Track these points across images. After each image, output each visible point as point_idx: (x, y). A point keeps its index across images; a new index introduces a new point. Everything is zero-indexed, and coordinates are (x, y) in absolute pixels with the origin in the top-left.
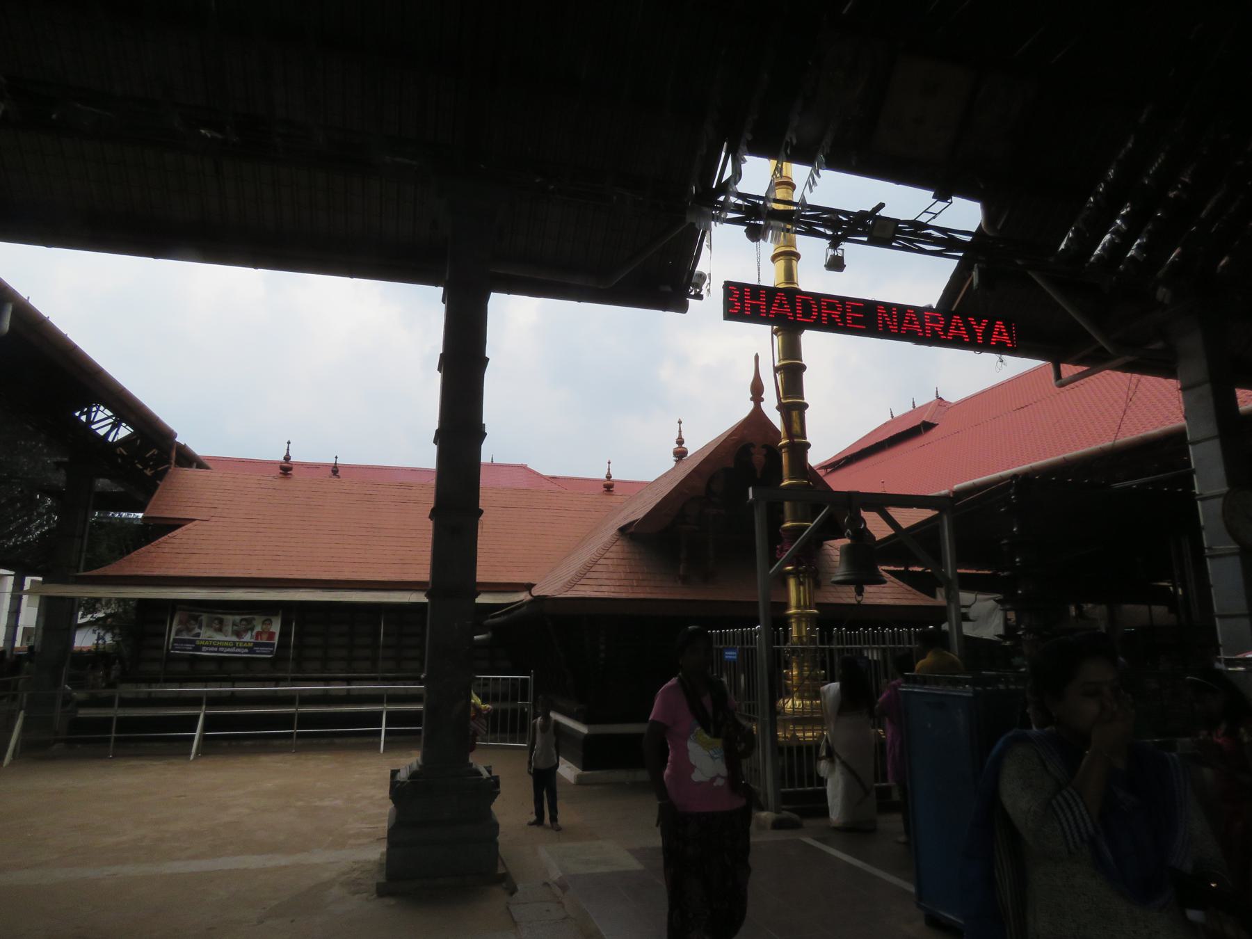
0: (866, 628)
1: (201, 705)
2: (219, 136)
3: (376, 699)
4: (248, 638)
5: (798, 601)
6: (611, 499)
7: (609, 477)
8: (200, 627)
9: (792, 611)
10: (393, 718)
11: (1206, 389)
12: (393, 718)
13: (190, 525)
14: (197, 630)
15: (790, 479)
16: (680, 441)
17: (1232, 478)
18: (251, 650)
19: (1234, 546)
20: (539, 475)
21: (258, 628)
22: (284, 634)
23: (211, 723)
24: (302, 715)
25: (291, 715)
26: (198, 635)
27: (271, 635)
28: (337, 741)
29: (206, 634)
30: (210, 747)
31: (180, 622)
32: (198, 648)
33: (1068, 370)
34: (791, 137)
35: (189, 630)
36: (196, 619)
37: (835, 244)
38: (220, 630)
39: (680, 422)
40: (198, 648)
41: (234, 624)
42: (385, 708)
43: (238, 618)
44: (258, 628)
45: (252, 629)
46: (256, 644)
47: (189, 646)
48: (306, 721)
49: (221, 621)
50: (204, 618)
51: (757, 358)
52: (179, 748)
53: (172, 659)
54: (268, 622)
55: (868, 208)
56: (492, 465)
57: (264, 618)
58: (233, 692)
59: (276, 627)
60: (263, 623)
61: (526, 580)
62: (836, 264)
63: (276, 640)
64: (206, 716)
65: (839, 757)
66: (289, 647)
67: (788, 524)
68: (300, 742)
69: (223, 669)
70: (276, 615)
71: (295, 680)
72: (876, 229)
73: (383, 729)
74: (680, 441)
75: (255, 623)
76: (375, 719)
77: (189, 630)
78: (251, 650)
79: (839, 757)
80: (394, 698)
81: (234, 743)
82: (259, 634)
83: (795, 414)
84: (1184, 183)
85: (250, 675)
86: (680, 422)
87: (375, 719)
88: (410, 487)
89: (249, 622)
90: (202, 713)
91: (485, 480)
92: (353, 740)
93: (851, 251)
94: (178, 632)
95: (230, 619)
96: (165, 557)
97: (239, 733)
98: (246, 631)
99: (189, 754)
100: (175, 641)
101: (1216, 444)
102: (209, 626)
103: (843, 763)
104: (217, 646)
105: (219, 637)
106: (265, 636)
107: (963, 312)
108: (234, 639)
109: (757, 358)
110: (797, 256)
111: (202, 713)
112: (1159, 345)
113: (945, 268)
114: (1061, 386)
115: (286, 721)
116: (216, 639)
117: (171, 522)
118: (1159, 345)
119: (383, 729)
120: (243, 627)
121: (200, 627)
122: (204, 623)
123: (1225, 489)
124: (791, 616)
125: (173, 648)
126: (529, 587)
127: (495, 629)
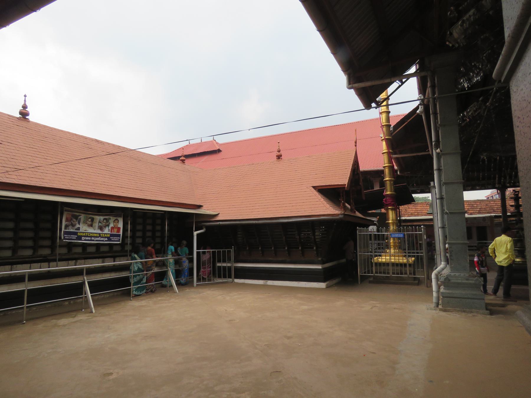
4: (106, 231)
18: (109, 239)
21: (112, 225)
26: (78, 229)
27: (119, 228)
29: (84, 228)
31: (67, 220)
35: (73, 225)
38: (91, 226)
40: (79, 238)
41: (100, 222)
43: (102, 218)
44: (112, 225)
45: (108, 226)
46: (112, 235)
49: (93, 220)
50: (82, 217)
53: (70, 246)
59: (121, 225)
60: (114, 222)
69: (99, 251)
75: (110, 221)
77: (73, 225)
82: (112, 228)
95: (98, 218)
97: (117, 289)
98: (105, 227)
102: (85, 222)
105: (90, 230)
106: (116, 230)
116: (90, 231)
125: (64, 239)
126: (199, 207)
127: (207, 228)
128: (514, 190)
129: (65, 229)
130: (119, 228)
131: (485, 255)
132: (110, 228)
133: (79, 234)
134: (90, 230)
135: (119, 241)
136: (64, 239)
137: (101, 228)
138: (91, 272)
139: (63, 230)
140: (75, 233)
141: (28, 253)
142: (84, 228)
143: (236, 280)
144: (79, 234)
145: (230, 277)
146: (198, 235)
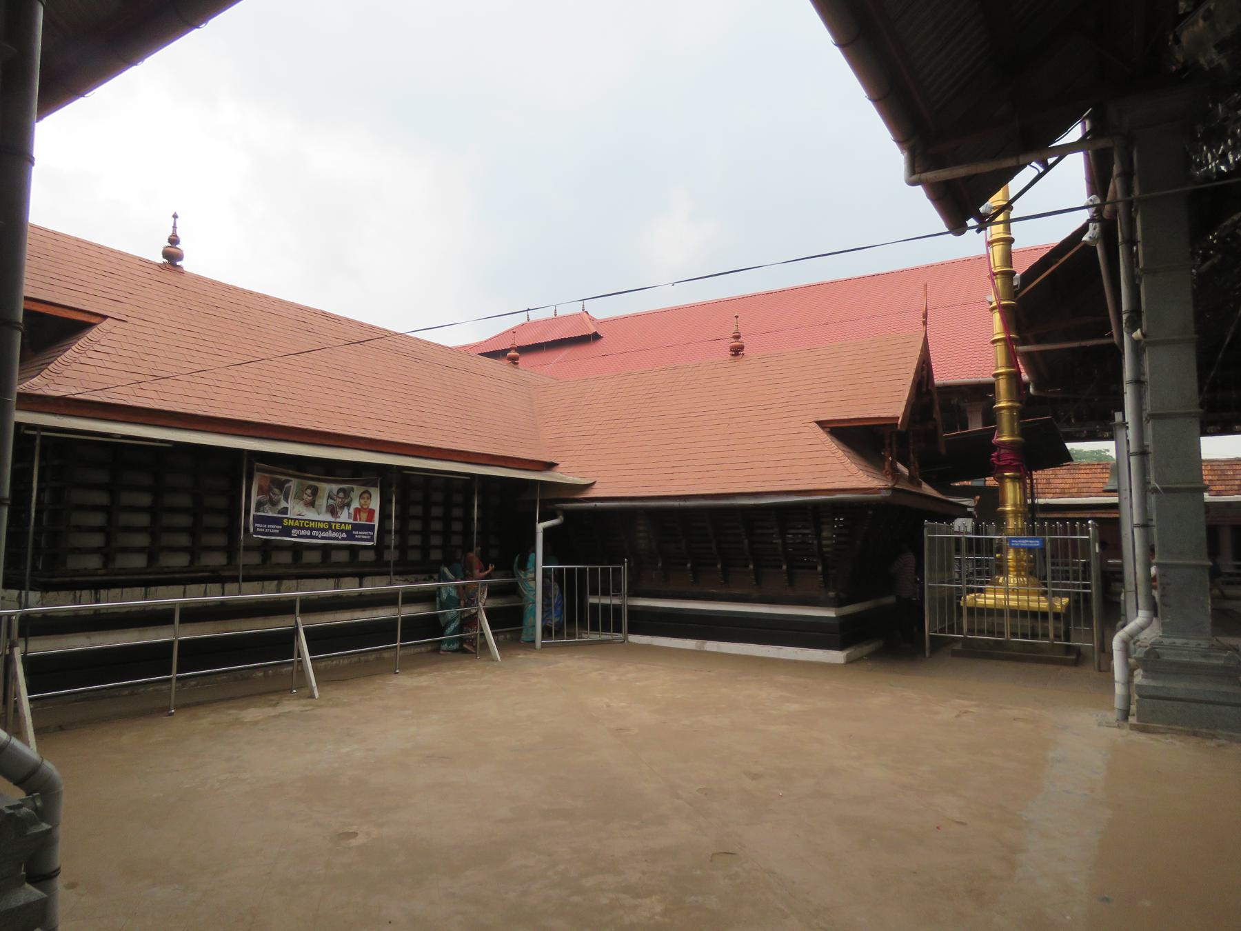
3: (285, 608)
4: (345, 517)
13: (106, 325)
14: (283, 504)
16: (174, 240)
18: (350, 536)
21: (356, 504)
22: (384, 516)
26: (285, 511)
27: (372, 512)
29: (296, 510)
31: (261, 491)
32: (287, 531)
35: (274, 503)
36: (281, 485)
38: (312, 504)
39: (175, 216)
40: (287, 531)
41: (330, 497)
42: (302, 623)
43: (335, 487)
44: (356, 504)
45: (348, 505)
46: (356, 527)
47: (276, 528)
48: (195, 654)
49: (315, 491)
50: (293, 484)
52: (294, 684)
54: (366, 495)
56: (32, 226)
57: (363, 489)
58: (96, 610)
61: (547, 458)
66: (390, 532)
69: (326, 562)
74: (174, 240)
75: (353, 495)
76: (282, 645)
77: (274, 503)
80: (311, 606)
82: (357, 511)
86: (175, 216)
91: (31, 246)
94: (260, 505)
95: (327, 488)
98: (342, 507)
102: (298, 497)
105: (310, 515)
106: (364, 515)
108: (329, 518)
116: (310, 515)
125: (256, 532)
126: (550, 466)
127: (568, 514)
129: (257, 510)
130: (372, 512)
132: (352, 510)
133: (286, 523)
134: (310, 515)
137: (333, 511)
139: (253, 512)
142: (296, 510)
144: (286, 523)
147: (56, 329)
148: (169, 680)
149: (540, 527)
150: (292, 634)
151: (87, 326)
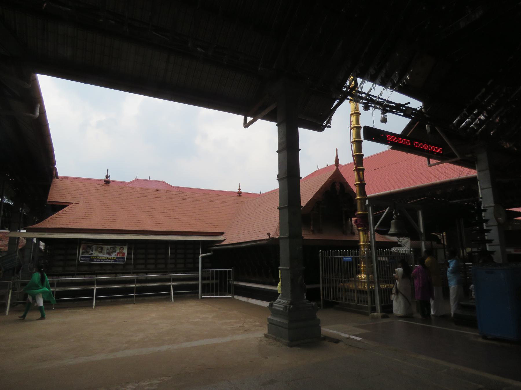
0: (343, 250)
1: (94, 285)
2: (203, 51)
3: (168, 280)
4: (113, 255)
5: (364, 240)
6: (240, 199)
7: (240, 190)
8: (92, 251)
9: (361, 244)
10: (176, 288)
11: (488, 172)
12: (176, 288)
13: (71, 206)
15: (360, 196)
17: (495, 202)
18: (115, 261)
19: (496, 223)
20: (170, 186)
21: (118, 251)
22: (129, 254)
23: (99, 292)
24: (137, 288)
25: (133, 288)
26: (92, 254)
27: (124, 254)
28: (146, 298)
29: (95, 254)
30: (101, 302)
31: (83, 249)
32: (92, 260)
33: (433, 161)
34: (372, 71)
35: (87, 252)
37: (383, 113)
38: (101, 252)
40: (92, 260)
41: (107, 250)
42: (172, 284)
43: (109, 247)
44: (118, 251)
45: (115, 252)
46: (117, 258)
48: (139, 290)
49: (102, 248)
50: (94, 247)
51: (337, 150)
52: (168, 297)
53: (80, 265)
55: (403, 103)
59: (125, 251)
60: (120, 249)
62: (384, 121)
63: (126, 256)
64: (97, 289)
65: (401, 293)
66: (131, 259)
67: (359, 213)
68: (137, 299)
69: (103, 268)
70: (125, 245)
71: (123, 273)
72: (387, 107)
73: (94, 297)
75: (116, 249)
77: (87, 252)
78: (115, 261)
79: (401, 293)
80: (175, 280)
81: (102, 301)
82: (118, 253)
83: (361, 173)
84: (493, 105)
85: (104, 272)
87: (168, 288)
88: (161, 191)
89: (114, 248)
90: (95, 288)
91: (56, 183)
92: (153, 298)
93: (389, 116)
95: (105, 247)
96: (59, 220)
97: (115, 295)
98: (113, 252)
99: (92, 306)
100: (82, 257)
101: (491, 189)
102: (96, 250)
103: (403, 295)
104: (100, 259)
105: (101, 255)
106: (121, 255)
107: (412, 139)
108: (108, 256)
109: (337, 150)
110: (360, 114)
111: (95, 288)
112: (470, 156)
113: (406, 121)
114: (431, 166)
115: (131, 290)
116: (100, 256)
117: (61, 204)
118: (470, 156)
119: (94, 297)
120: (111, 251)
121: (92, 251)
122: (94, 249)
123: (493, 205)
124: (361, 245)
125: (81, 260)
126: (222, 234)
127: (215, 251)
128: (125, 253)
129: (82, 254)
130: (124, 254)
131: (355, 281)
132: (116, 253)
133: (91, 258)
134: (101, 255)
135: (124, 261)
136: (81, 260)
137: (109, 254)
138: (99, 283)
139: (80, 255)
140: (89, 257)
141: (153, 266)
142: (95, 254)
143: (236, 297)
144: (91, 258)
145: (230, 293)
146: (203, 257)
147: (59, 207)
148: (132, 297)
149: (201, 256)
150: (170, 286)
151: (67, 206)
